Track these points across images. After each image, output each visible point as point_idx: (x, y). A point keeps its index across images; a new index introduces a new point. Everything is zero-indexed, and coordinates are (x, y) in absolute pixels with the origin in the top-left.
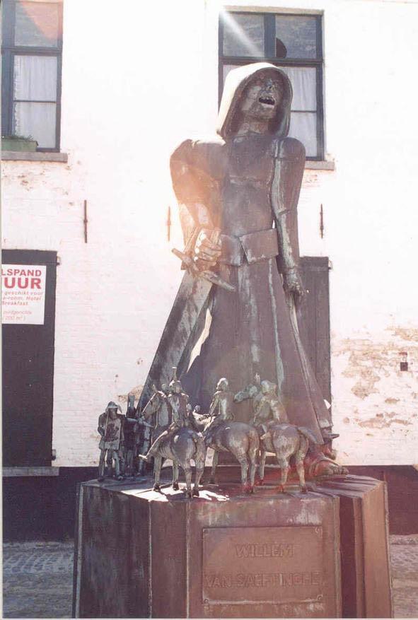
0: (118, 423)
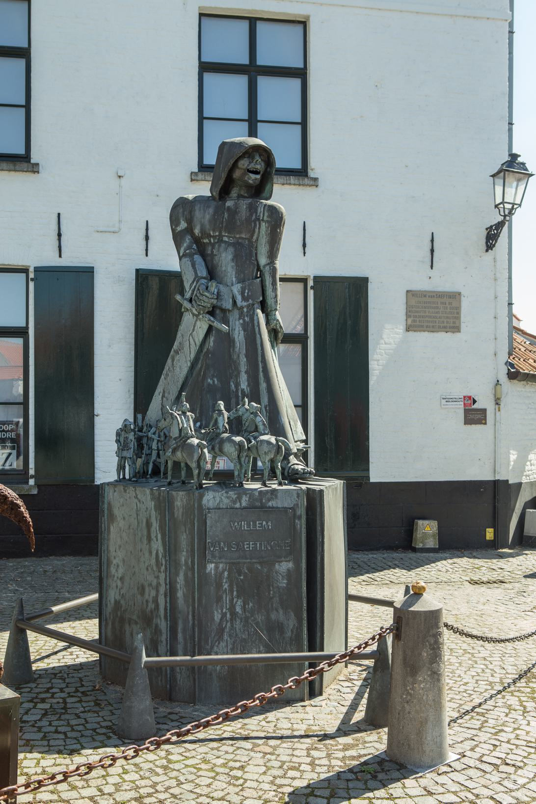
0: (131, 436)
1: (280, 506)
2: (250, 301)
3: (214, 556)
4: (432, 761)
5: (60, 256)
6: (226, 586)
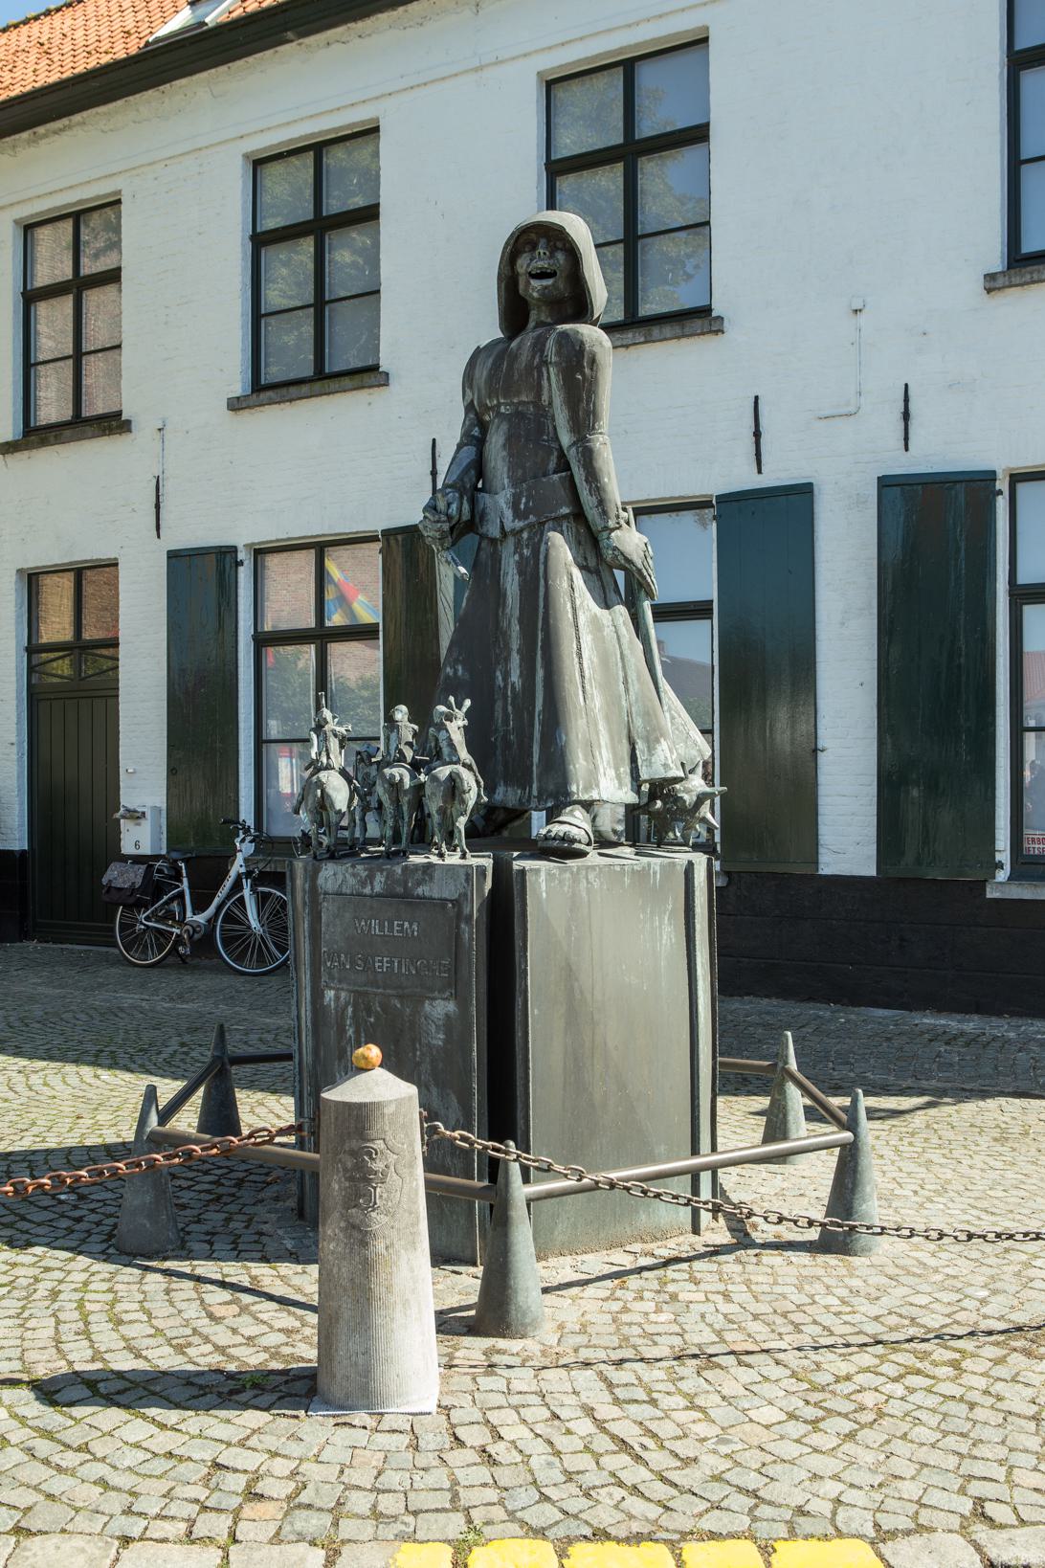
1: (436, 895)
2: (532, 518)
3: (331, 977)
4: (347, 1396)
5: (760, 472)
6: (350, 1032)
